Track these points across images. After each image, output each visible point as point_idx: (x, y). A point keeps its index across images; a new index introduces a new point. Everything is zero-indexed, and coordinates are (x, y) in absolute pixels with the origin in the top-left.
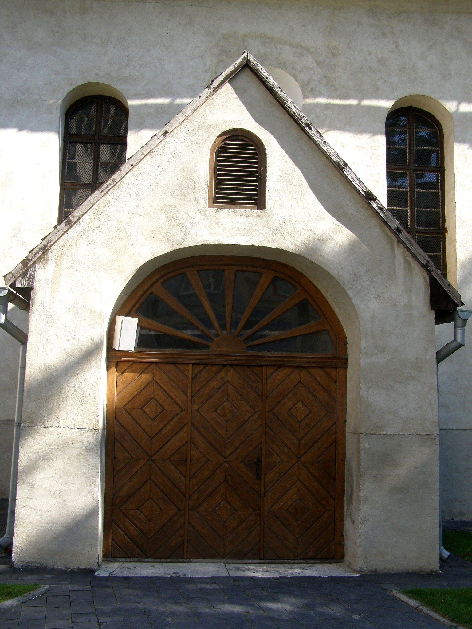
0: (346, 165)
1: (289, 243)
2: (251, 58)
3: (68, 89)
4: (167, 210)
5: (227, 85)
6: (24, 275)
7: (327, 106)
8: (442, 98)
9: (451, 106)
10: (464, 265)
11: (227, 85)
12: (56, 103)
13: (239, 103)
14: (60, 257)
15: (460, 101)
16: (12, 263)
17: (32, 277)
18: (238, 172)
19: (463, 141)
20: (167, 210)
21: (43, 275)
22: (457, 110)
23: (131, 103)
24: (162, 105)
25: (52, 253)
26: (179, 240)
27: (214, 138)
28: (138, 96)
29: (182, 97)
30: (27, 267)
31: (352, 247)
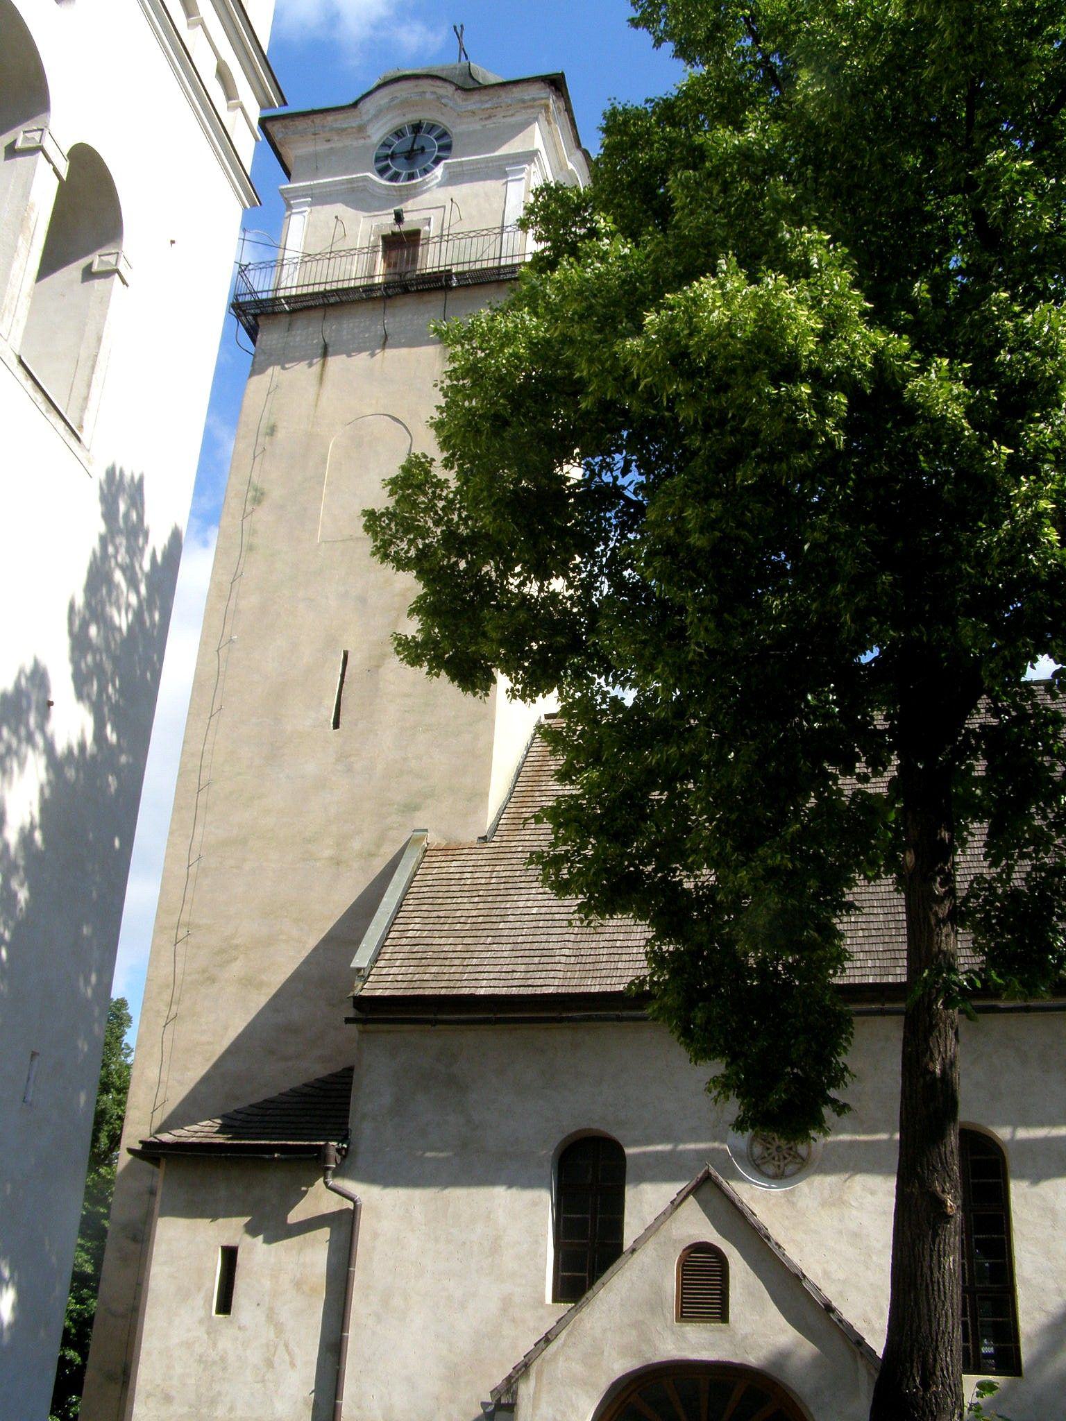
0: (804, 1276)
1: (753, 1358)
2: (712, 1171)
3: (560, 1137)
4: (636, 1325)
5: (691, 1198)
6: (508, 1391)
7: (852, 1144)
8: (993, 1124)
9: (1003, 1133)
10: (1029, 1339)
11: (691, 1198)
12: (547, 1152)
13: (702, 1215)
14: (540, 1373)
15: (1015, 1126)
16: (498, 1379)
17: (515, 1393)
18: (702, 1285)
19: (1022, 1177)
20: (636, 1325)
21: (526, 1390)
22: (1013, 1137)
23: (629, 1151)
24: (662, 1152)
25: (533, 1370)
26: (649, 1355)
27: (679, 1252)
28: (636, 1143)
29: (685, 1142)
30: (510, 1385)
31: (816, 1363)
